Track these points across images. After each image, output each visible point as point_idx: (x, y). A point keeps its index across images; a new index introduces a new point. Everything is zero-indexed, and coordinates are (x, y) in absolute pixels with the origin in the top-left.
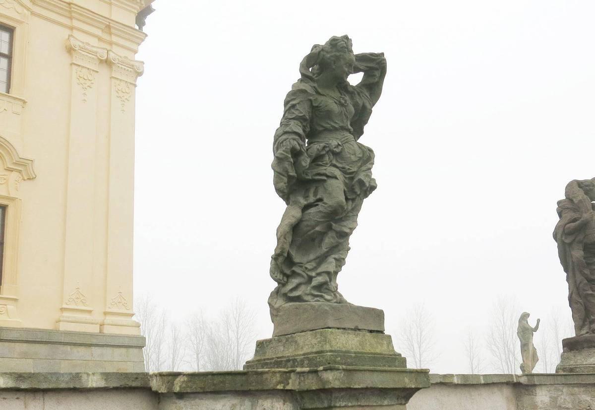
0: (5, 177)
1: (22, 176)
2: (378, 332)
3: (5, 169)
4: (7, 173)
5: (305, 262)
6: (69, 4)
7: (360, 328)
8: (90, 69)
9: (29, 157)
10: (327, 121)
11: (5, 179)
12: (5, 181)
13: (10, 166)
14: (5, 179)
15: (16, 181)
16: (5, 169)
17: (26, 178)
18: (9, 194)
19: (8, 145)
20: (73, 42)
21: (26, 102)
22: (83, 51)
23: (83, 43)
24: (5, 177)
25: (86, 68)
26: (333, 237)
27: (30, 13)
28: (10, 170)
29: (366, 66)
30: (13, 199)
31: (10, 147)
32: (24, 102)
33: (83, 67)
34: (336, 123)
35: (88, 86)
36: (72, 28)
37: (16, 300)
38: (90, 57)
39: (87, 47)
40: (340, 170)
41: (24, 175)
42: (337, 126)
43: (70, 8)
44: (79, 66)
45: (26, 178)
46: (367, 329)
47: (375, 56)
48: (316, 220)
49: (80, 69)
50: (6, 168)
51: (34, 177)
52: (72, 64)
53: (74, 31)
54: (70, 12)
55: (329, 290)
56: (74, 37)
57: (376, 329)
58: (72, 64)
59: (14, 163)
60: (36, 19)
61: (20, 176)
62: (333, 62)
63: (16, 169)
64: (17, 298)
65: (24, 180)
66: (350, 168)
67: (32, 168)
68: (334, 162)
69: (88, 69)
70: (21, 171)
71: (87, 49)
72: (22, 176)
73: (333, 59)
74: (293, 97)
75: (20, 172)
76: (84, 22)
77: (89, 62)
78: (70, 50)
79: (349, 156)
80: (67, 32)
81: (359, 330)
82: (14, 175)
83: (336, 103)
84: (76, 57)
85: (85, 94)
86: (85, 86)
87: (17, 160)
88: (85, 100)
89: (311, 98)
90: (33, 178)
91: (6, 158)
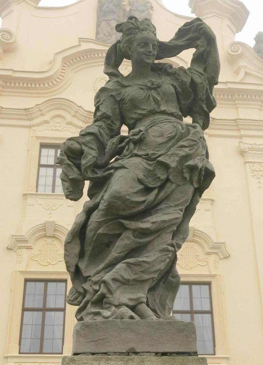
0: (206, 260)
1: (219, 256)
2: (189, 354)
3: (205, 254)
4: (207, 256)
5: (92, 274)
6: (235, 120)
7: (138, 351)
8: (261, 162)
9: (222, 241)
10: (135, 111)
11: (206, 262)
12: (206, 263)
13: (208, 251)
14: (206, 262)
15: (215, 261)
16: (205, 254)
17: (222, 258)
18: (210, 272)
19: (202, 234)
20: (242, 146)
21: (214, 200)
22: (252, 151)
23: (251, 145)
24: (206, 260)
25: (257, 162)
26: (128, 238)
27: (208, 136)
28: (209, 254)
29: (185, 41)
30: (214, 276)
31: (207, 237)
32: (213, 201)
33: (254, 162)
34: (144, 109)
35: (261, 176)
36: (241, 137)
37: (227, 358)
38: (259, 154)
39: (254, 146)
40: (143, 158)
41: (220, 256)
42: (144, 112)
43: (237, 126)
44: (251, 162)
45: (222, 258)
46: (153, 351)
47: (189, 25)
48: (96, 222)
49: (252, 164)
50: (206, 253)
51: (228, 255)
52: (246, 163)
53: (243, 138)
54: (237, 126)
55: (110, 304)
56: (243, 143)
57: (176, 350)
58: (246, 163)
59: (211, 248)
60: (215, 139)
61: (217, 257)
62: (128, 49)
63: (212, 252)
64: (229, 357)
65: (221, 259)
66: (156, 152)
67: (225, 247)
68: (135, 152)
69: (259, 162)
70: (217, 253)
71: (256, 148)
72: (219, 256)
73: (126, 45)
74: (98, 100)
75: (216, 253)
76: (220, 129)
77: (253, 157)
78: (242, 153)
79: (153, 139)
80: (236, 142)
81: (136, 353)
82: (213, 257)
83: (142, 89)
84: (247, 157)
85: (259, 182)
86: (259, 176)
87: (213, 245)
88: (260, 187)
89: (113, 93)
90: (227, 257)
91: (205, 245)
